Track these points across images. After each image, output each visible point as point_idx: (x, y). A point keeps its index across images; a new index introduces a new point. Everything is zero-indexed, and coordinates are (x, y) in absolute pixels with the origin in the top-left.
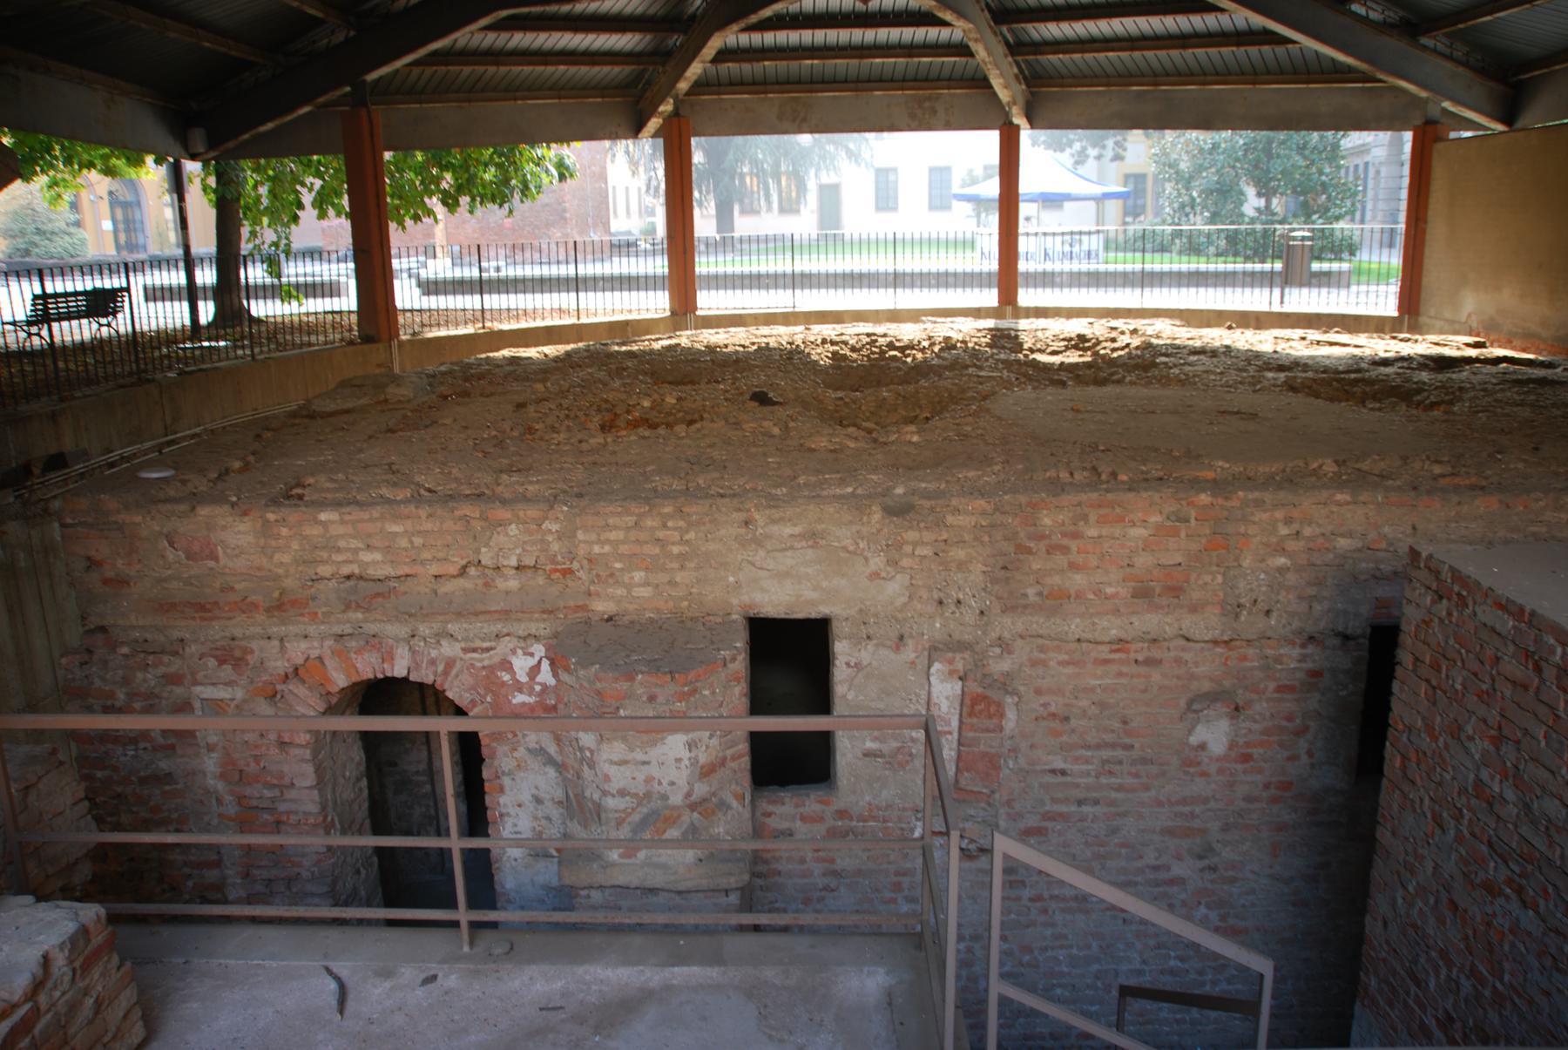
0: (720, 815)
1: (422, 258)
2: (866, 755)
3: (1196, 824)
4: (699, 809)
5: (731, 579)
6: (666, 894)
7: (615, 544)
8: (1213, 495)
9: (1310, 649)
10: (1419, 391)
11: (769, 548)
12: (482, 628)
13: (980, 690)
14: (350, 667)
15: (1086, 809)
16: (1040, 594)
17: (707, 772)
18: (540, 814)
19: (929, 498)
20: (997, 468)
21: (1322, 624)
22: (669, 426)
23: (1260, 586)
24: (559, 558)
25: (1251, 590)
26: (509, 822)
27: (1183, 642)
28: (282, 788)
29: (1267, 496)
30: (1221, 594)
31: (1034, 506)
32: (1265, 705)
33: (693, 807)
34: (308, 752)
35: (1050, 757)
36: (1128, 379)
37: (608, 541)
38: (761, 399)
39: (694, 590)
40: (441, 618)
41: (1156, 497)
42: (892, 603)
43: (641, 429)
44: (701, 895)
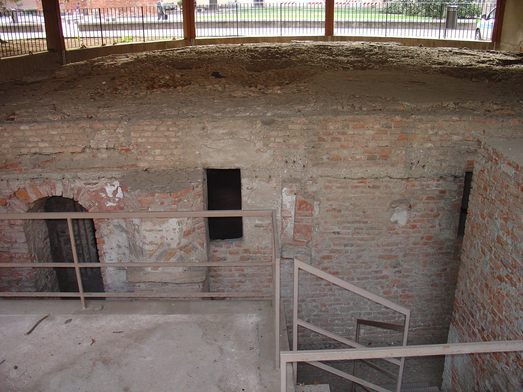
0: (193, 252)
1: (82, 15)
2: (256, 226)
3: (393, 254)
4: (184, 250)
5: (197, 152)
6: (171, 284)
7: (147, 138)
8: (402, 117)
9: (441, 182)
10: (494, 74)
11: (213, 139)
12: (92, 174)
13: (303, 199)
14: (37, 192)
15: (348, 248)
16: (329, 158)
17: (187, 234)
18: (120, 252)
19: (281, 117)
20: (312, 105)
21: (446, 172)
22: (175, 87)
23: (421, 155)
24: (124, 144)
25: (417, 157)
26: (107, 256)
27: (389, 179)
28: (12, 243)
29: (424, 117)
30: (404, 158)
31: (326, 121)
32: (422, 205)
33: (181, 249)
34: (22, 228)
35: (333, 227)
36: (375, 67)
37: (144, 137)
38: (216, 75)
39: (181, 157)
40: (75, 171)
41: (378, 117)
42: (266, 162)
43: (163, 88)
44: (186, 285)
